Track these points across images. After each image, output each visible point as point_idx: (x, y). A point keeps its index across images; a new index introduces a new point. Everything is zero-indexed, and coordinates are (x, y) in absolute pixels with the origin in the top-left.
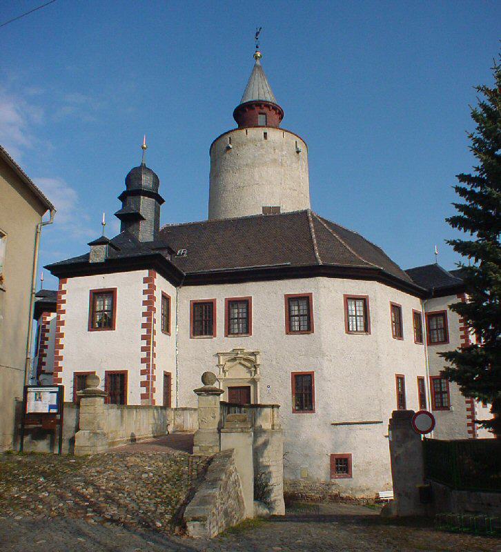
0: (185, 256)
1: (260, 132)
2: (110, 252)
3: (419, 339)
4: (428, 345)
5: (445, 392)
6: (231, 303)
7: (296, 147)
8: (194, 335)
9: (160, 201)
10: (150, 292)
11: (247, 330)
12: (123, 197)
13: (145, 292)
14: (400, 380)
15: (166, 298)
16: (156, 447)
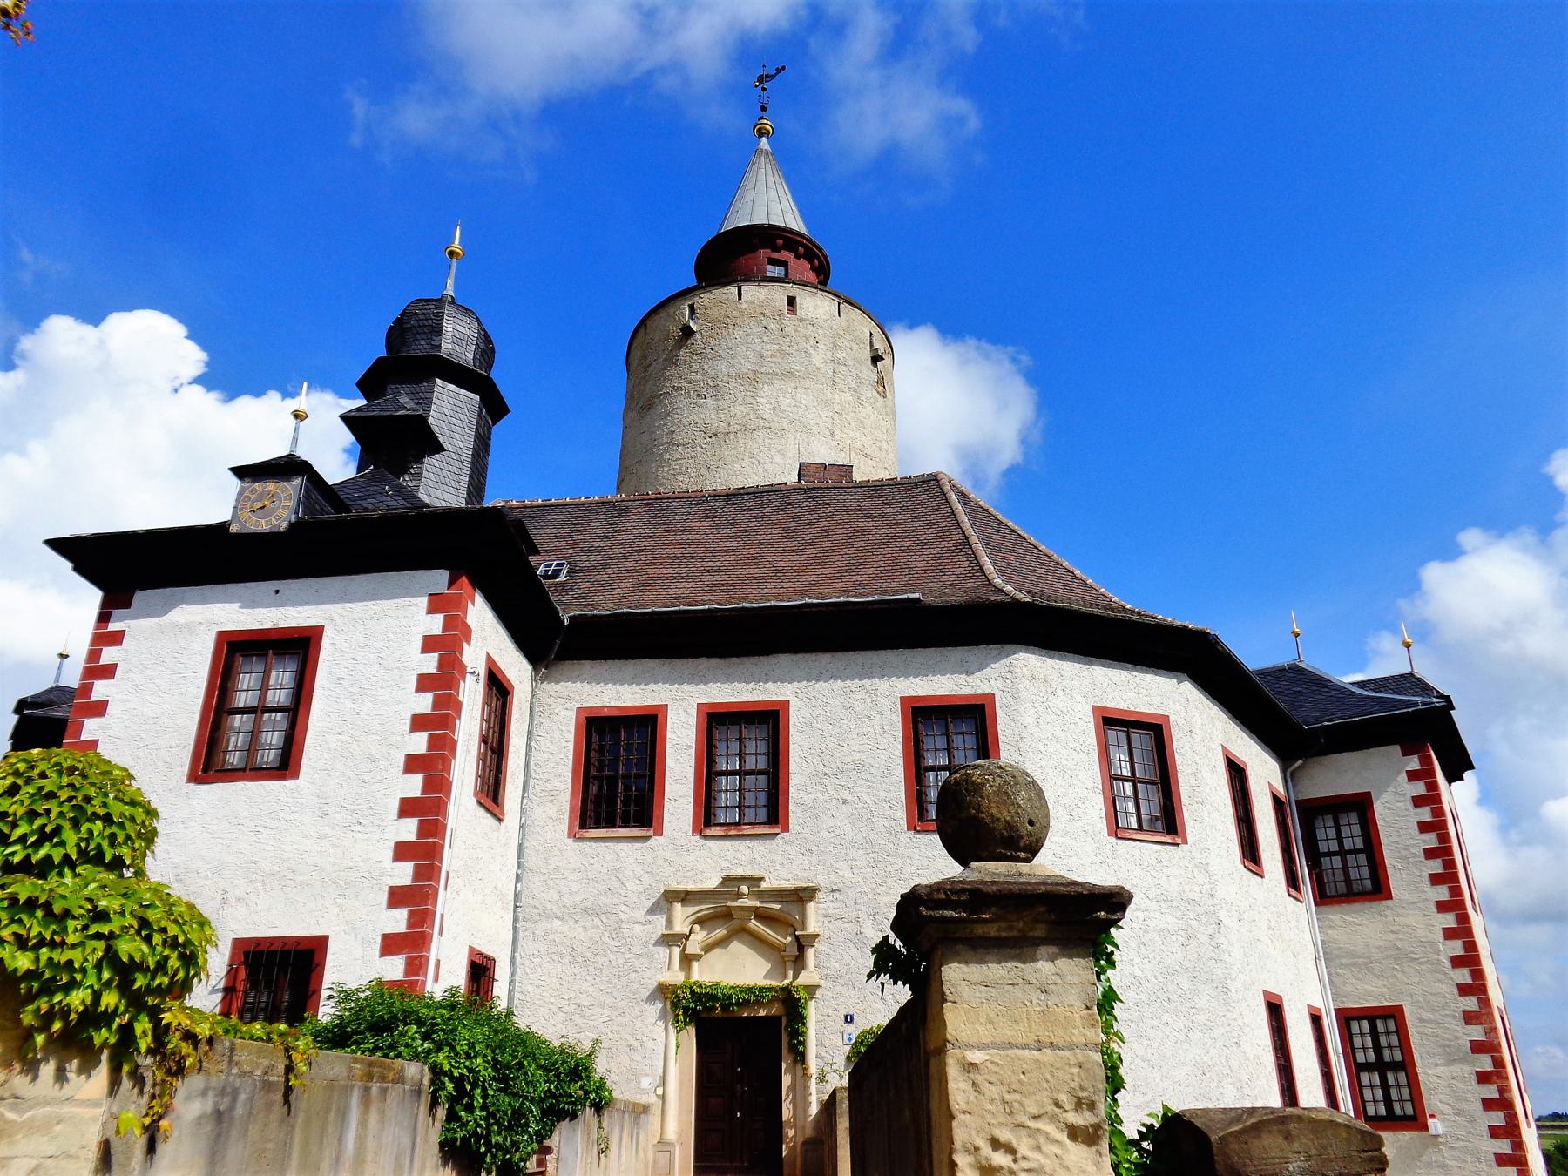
0: (563, 577)
1: (775, 295)
2: (308, 505)
3: (1292, 881)
4: (1316, 904)
5: (1367, 1067)
6: (716, 720)
7: (871, 344)
8: (583, 826)
9: (494, 407)
10: (447, 645)
11: (775, 814)
12: (371, 384)
13: (429, 644)
14: (1275, 1010)
15: (498, 687)
16: (1120, 996)
